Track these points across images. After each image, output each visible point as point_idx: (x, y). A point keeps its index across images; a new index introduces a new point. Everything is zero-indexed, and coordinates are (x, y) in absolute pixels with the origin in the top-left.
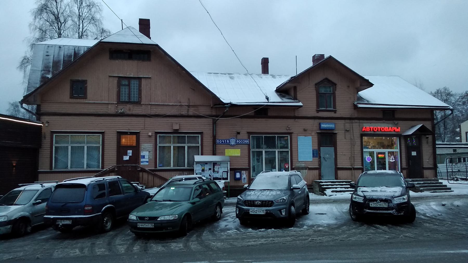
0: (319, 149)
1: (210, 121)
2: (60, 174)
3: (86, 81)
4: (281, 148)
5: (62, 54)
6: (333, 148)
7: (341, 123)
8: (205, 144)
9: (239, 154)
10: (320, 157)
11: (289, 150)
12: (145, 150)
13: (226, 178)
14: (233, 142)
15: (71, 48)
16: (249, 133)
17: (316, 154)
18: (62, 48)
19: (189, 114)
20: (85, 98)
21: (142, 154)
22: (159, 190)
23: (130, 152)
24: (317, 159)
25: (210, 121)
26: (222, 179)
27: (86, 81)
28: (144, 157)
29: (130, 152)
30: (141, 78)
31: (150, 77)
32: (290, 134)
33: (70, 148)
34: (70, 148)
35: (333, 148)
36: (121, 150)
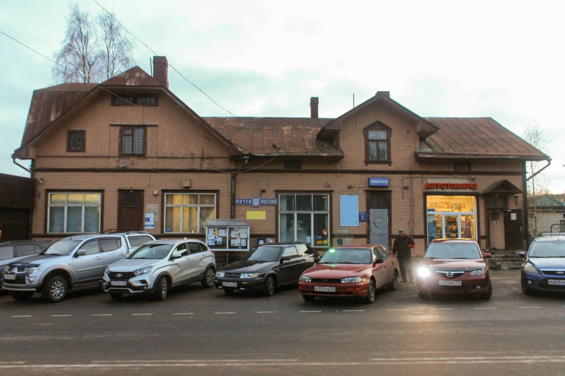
0: (368, 212)
6: (386, 211)
14: (256, 202)
16: (277, 192)
24: (365, 224)
25: (228, 176)
26: (277, 148)
32: (331, 192)
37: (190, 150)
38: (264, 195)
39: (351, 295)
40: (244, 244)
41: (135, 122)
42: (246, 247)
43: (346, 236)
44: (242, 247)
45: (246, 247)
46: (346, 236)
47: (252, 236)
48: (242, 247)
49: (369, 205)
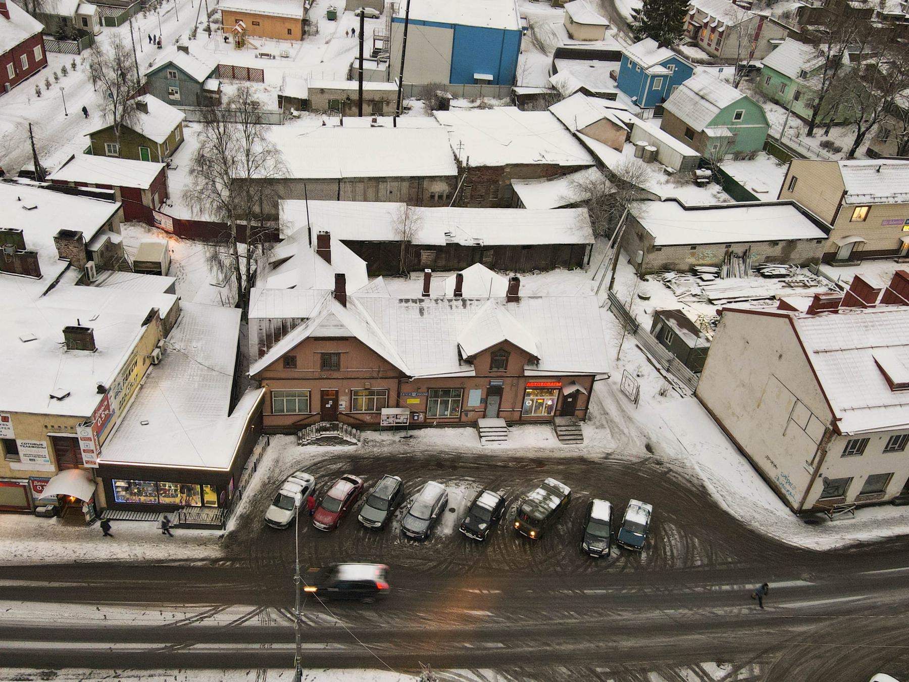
0: (487, 398)
1: (396, 380)
2: (812, 374)
3: (296, 356)
4: (455, 396)
5: (272, 327)
6: (499, 397)
7: (509, 380)
8: (391, 396)
9: (419, 402)
10: (487, 403)
11: (461, 399)
12: (342, 400)
13: (769, 153)
14: (414, 394)
15: (279, 320)
16: (428, 388)
17: (484, 401)
18: (272, 321)
19: (212, 249)
20: (296, 367)
21: (340, 403)
22: (693, 321)
23: (331, 402)
24: (483, 405)
25: (396, 380)
26: (440, 393)
27: (296, 356)
28: (342, 405)
29: (331, 402)
30: (340, 353)
31: (347, 351)
32: (464, 389)
33: (297, 400)
34: (297, 400)
35: (499, 397)
36: (323, 402)
37: (323, 566)
38: (419, 391)
39: (548, 648)
40: (405, 421)
41: (520, 75)
42: (406, 423)
43: (470, 411)
44: (404, 423)
45: (406, 423)
46: (470, 411)
47: (411, 412)
48: (404, 423)
49: (488, 395)
